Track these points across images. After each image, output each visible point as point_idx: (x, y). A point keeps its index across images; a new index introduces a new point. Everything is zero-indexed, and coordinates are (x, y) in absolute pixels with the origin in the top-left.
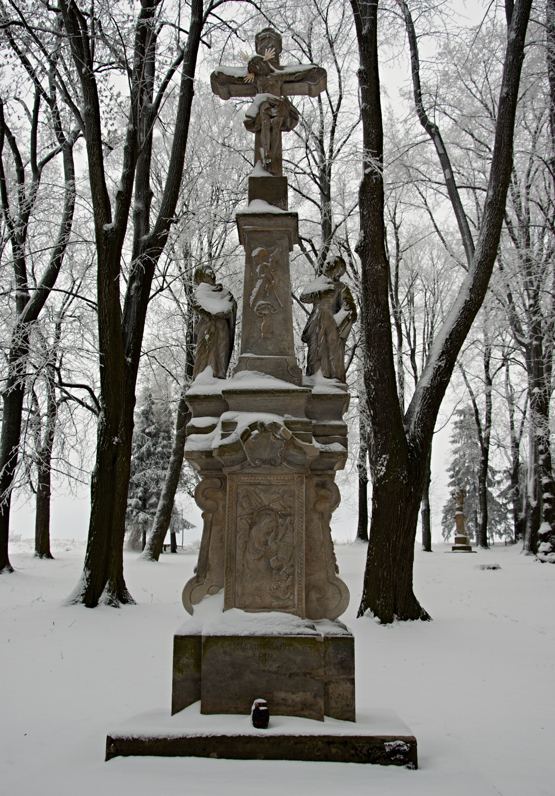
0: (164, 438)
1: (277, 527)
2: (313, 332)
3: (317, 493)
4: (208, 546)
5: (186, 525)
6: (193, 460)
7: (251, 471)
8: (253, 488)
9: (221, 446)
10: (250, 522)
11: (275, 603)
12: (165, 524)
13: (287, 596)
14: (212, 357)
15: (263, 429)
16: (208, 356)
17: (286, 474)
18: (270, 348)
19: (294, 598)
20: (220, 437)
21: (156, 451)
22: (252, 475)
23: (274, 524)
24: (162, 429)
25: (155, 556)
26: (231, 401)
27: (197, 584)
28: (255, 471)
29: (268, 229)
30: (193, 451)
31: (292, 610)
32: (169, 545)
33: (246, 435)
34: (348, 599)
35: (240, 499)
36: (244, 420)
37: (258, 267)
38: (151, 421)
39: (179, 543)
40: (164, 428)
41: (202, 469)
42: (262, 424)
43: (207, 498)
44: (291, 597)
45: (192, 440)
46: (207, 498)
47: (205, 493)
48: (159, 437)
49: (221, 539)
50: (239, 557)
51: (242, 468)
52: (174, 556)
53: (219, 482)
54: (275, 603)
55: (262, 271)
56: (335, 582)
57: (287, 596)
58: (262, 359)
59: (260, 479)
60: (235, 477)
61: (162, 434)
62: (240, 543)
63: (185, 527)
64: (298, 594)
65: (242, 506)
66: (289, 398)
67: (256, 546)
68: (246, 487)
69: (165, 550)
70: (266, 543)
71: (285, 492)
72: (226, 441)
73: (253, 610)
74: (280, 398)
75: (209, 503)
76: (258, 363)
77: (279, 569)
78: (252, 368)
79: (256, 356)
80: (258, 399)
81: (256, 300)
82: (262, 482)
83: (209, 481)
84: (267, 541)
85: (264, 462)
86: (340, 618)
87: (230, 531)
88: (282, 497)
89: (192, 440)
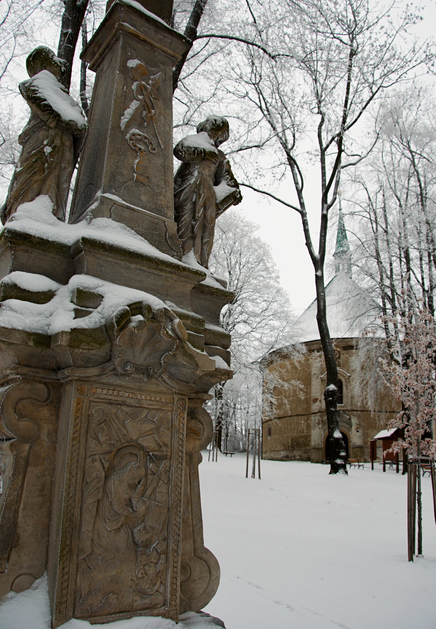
1: (146, 475)
2: (187, 198)
4: (18, 502)
7: (113, 380)
8: (113, 410)
9: (74, 330)
10: (106, 466)
11: (139, 602)
13: (156, 588)
14: (51, 182)
15: (150, 316)
16: (44, 181)
17: (161, 392)
18: (143, 198)
20: (73, 314)
22: (114, 387)
23: (142, 472)
26: (88, 259)
28: (119, 382)
29: (153, 42)
30: (14, 330)
31: (162, 610)
33: (123, 318)
34: (218, 578)
36: (117, 297)
37: (135, 84)
42: (149, 308)
43: (21, 416)
44: (161, 590)
45: (12, 309)
46: (21, 416)
47: (20, 406)
49: (42, 490)
50: (86, 528)
53: (45, 390)
55: (141, 89)
56: (204, 556)
58: (132, 209)
59: (125, 395)
62: (90, 500)
65: (97, 439)
66: (175, 277)
67: (115, 507)
68: (103, 406)
70: (129, 503)
72: (84, 323)
74: (163, 274)
76: (127, 214)
77: (147, 545)
78: (119, 219)
79: (124, 202)
80: (133, 266)
81: (129, 125)
82: (128, 401)
83: (28, 386)
84: (130, 500)
85: (138, 369)
87: (73, 480)
88: (158, 428)
89: (12, 309)
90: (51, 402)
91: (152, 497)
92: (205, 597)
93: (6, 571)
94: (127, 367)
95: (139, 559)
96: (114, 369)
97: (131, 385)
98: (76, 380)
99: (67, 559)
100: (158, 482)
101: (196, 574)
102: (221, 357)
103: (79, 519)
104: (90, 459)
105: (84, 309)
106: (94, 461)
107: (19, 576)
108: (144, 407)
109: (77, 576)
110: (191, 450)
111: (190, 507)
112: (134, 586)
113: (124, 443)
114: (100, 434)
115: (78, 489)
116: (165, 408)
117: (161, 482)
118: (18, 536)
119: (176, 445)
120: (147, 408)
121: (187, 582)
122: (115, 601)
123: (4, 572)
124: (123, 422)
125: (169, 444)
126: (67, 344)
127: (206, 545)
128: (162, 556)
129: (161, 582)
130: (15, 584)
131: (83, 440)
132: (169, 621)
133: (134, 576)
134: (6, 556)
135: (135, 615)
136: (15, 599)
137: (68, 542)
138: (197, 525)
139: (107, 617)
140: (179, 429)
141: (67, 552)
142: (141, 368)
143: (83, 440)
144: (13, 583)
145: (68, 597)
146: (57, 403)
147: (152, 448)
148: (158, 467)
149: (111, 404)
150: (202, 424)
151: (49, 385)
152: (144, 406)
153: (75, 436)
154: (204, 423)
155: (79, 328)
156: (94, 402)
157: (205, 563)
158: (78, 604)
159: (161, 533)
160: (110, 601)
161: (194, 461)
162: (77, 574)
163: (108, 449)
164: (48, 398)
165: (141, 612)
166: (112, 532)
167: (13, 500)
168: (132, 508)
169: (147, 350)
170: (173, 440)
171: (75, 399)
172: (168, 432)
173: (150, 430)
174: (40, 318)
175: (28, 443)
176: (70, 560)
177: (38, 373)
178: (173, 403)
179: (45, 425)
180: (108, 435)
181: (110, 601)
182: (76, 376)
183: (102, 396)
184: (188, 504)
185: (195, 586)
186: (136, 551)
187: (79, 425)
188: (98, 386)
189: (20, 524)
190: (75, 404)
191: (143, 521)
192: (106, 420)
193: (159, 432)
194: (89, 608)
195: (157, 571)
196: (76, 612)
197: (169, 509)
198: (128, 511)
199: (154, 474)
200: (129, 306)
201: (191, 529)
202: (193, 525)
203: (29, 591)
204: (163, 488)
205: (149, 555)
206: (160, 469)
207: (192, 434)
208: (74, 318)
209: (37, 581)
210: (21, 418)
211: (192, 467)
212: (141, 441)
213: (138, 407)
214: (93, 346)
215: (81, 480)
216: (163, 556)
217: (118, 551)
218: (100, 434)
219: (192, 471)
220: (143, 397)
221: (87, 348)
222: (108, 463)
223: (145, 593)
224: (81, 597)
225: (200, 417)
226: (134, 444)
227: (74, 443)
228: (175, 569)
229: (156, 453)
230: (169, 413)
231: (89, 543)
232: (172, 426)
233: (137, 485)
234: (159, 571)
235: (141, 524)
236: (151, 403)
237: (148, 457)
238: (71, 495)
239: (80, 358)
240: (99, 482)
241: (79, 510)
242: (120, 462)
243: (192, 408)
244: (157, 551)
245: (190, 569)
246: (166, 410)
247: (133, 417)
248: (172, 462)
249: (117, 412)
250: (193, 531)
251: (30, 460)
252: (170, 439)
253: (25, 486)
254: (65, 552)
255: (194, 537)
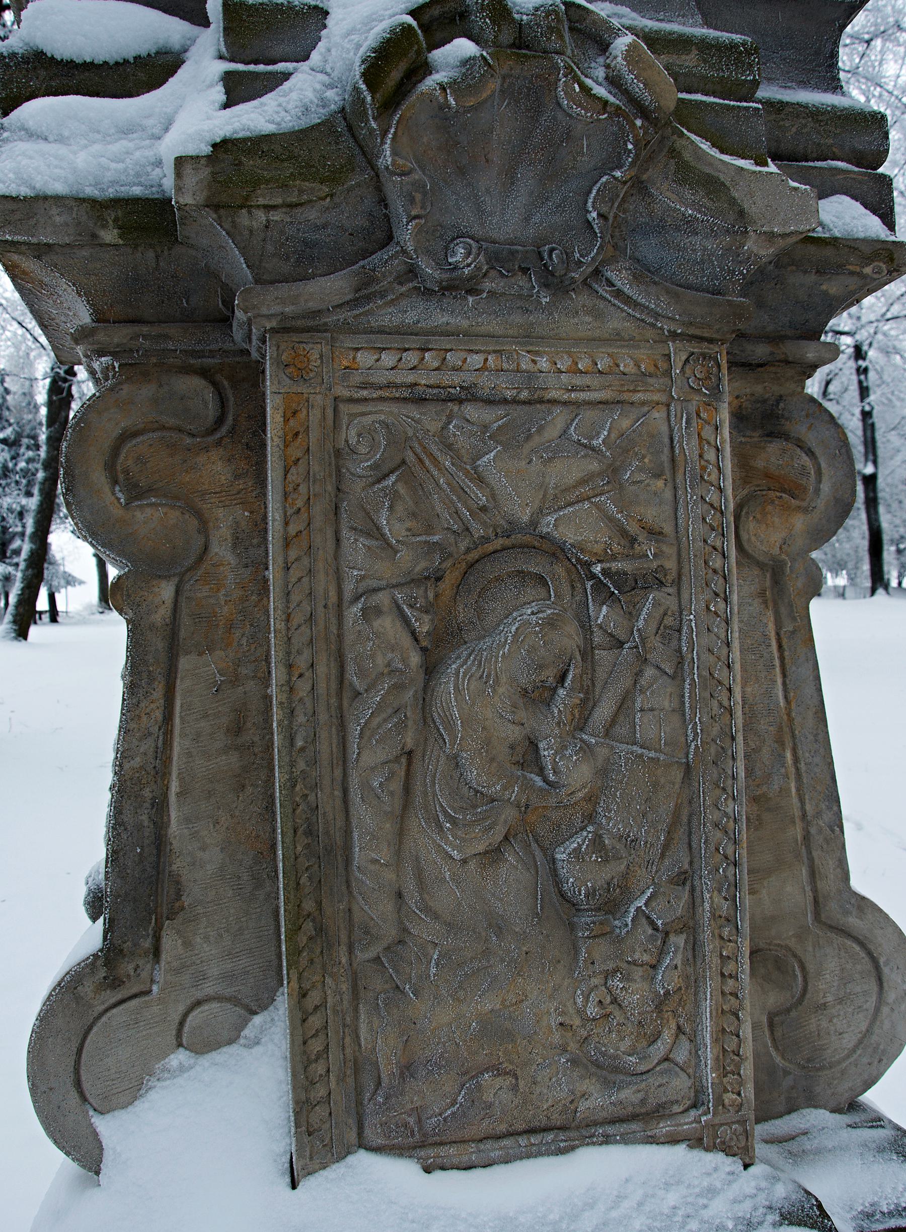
0: (28, 448)
1: (587, 652)
3: (743, 461)
4: (162, 773)
5: (70, 581)
6: (41, 251)
7: (413, 313)
8: (429, 420)
10: (423, 626)
11: (596, 1100)
12: (35, 581)
13: (660, 1049)
15: (507, 37)
17: (617, 338)
19: (695, 1053)
20: (218, 94)
21: (18, 468)
23: (569, 637)
24: (25, 434)
25: (22, 633)
27: (112, 997)
28: (441, 319)
31: (687, 1122)
32: (46, 612)
35: (356, 488)
38: (7, 421)
39: (60, 607)
40: (27, 430)
41: (100, 317)
43: (136, 492)
44: (681, 1055)
45: (31, 135)
46: (136, 492)
47: (126, 459)
48: (20, 445)
49: (237, 729)
50: (369, 851)
51: (364, 293)
52: (53, 629)
53: (209, 395)
54: (596, 1100)
56: (853, 921)
57: (660, 1049)
59: (471, 365)
60: (315, 351)
61: (25, 441)
62: (371, 759)
63: (68, 583)
64: (721, 1033)
65: (374, 532)
68: (388, 412)
69: (40, 618)
70: (528, 755)
71: (624, 446)
72: (258, 117)
73: (471, 1152)
75: (151, 519)
77: (611, 902)
82: (486, 383)
83: (147, 391)
84: (533, 745)
85: (501, 258)
86: (873, 1097)
87: (302, 688)
88: (613, 472)
90: (232, 431)
91: (621, 730)
92: (865, 1060)
93: (155, 988)
94: (454, 254)
95: (583, 954)
96: (412, 272)
97: (490, 324)
98: (273, 331)
99: (312, 961)
100: (639, 674)
101: (826, 985)
102: (855, 198)
103: (340, 823)
104: (356, 609)
105: (261, 68)
106: (368, 614)
107: (198, 1003)
108: (554, 402)
109: (356, 1018)
110: (776, 551)
111: (789, 755)
112: (573, 1046)
113: (485, 540)
114: (384, 513)
115: (323, 717)
116: (639, 397)
117: (649, 672)
118: (178, 883)
119: (694, 529)
120: (565, 403)
121: (793, 1014)
122: (506, 1096)
123: (149, 992)
124: (475, 459)
125: (668, 529)
126: (201, 198)
127: (858, 883)
128: (673, 938)
129: (680, 1030)
130: (186, 1029)
131: (323, 541)
132: (717, 1159)
133: (571, 1011)
134: (147, 944)
135: (588, 1140)
136: (192, 1073)
137: (309, 906)
138: (818, 814)
139: (482, 1146)
140: (704, 469)
141: (311, 938)
142: (513, 253)
143: (323, 541)
144: (182, 1024)
145: (333, 1085)
146: (254, 433)
147: (598, 548)
148: (632, 616)
149: (421, 400)
150: (810, 453)
151: (218, 377)
152: (553, 394)
153: (292, 530)
154: (818, 452)
155: (241, 135)
156: (351, 400)
157: (857, 948)
158: (369, 1108)
159: (663, 855)
160: (488, 1097)
161: (787, 592)
162: (356, 1010)
163: (423, 564)
164: (220, 421)
165: (610, 1130)
166: (472, 865)
167: (141, 767)
168: (541, 771)
169: (527, 180)
170: (681, 511)
171: (278, 399)
172: (660, 483)
173: (583, 482)
174: (131, 145)
175: (167, 578)
176: (324, 967)
177: (166, 337)
178: (668, 373)
179: (220, 513)
180: (414, 515)
181: (488, 1097)
182: (269, 317)
183: (380, 378)
184: (782, 744)
185: (824, 1024)
186: (572, 927)
187: (303, 489)
188: (360, 340)
189: (176, 844)
190: (279, 419)
191: (590, 818)
192: (404, 462)
193: (621, 487)
194: (411, 1120)
195: (657, 994)
196: (368, 1132)
197: (688, 769)
198: (528, 786)
199: (621, 644)
200: (413, 13)
201: (798, 831)
202: (804, 815)
203: (233, 1049)
204: (657, 695)
205: (620, 940)
206: (641, 623)
207: (772, 494)
208: (226, 106)
209: (257, 1020)
210: (139, 497)
211: (783, 611)
212: (548, 524)
213: (528, 402)
214: (301, 191)
215: (334, 686)
216: (679, 940)
217: (499, 931)
218: (384, 513)
219: (788, 627)
220: (544, 363)
221: (279, 201)
222: (426, 618)
223: (616, 1070)
224: (379, 1084)
225: (800, 429)
226: (528, 539)
227: (293, 554)
228: (731, 982)
229: (616, 566)
230: (658, 415)
231: (388, 907)
232: (673, 460)
233: (554, 690)
234: (667, 993)
235: (583, 829)
236: (578, 381)
237: (589, 585)
238: (300, 743)
239: (270, 248)
240: (398, 687)
241: (338, 793)
242: (480, 613)
243: (765, 401)
244: (652, 923)
245: (803, 968)
246: (643, 403)
247: (511, 439)
248: (685, 596)
249: (445, 427)
250: (807, 837)
251: (183, 634)
252: (668, 509)
253: (177, 720)
254: (303, 939)
255: (811, 860)
